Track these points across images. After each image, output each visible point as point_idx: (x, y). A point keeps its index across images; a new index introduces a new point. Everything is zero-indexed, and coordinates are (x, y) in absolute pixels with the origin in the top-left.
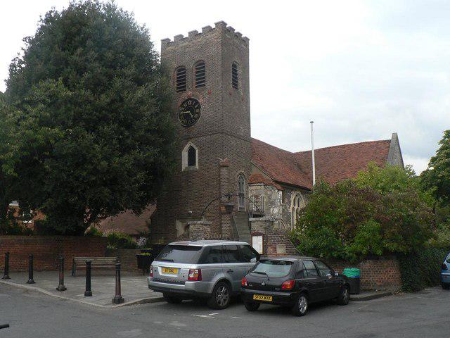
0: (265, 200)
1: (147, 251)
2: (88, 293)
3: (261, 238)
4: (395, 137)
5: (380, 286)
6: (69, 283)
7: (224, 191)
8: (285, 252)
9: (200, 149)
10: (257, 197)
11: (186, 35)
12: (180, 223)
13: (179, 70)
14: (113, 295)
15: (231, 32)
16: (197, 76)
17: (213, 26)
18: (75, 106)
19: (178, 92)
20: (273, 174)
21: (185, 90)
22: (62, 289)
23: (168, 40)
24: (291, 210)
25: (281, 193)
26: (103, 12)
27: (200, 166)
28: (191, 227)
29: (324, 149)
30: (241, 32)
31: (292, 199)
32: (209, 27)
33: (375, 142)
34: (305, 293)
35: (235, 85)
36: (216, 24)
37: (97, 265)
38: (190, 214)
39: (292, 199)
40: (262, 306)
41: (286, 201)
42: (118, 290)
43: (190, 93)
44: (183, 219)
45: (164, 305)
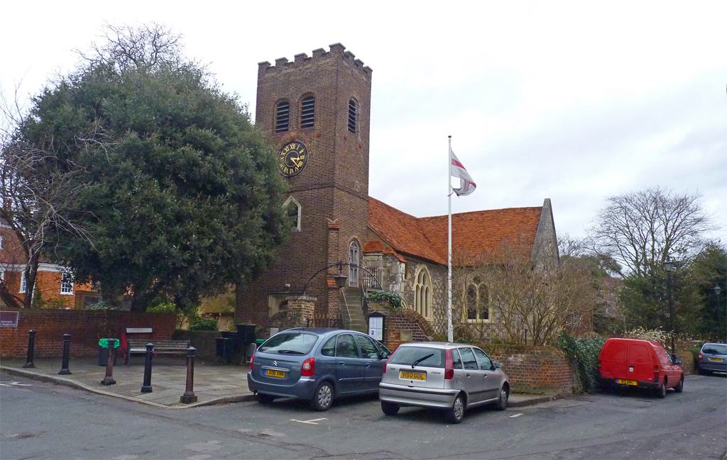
0: (383, 274)
2: (147, 388)
3: (381, 320)
4: (548, 202)
5: (535, 388)
6: (117, 374)
7: (331, 261)
10: (373, 270)
11: (291, 59)
12: (274, 300)
13: (281, 104)
14: (181, 389)
15: (350, 58)
16: (304, 113)
17: (328, 50)
18: (267, 192)
19: (277, 132)
20: (395, 242)
21: (287, 130)
22: (108, 382)
24: (414, 289)
25: (403, 265)
27: (303, 225)
28: (290, 303)
30: (353, 52)
31: (417, 275)
33: (521, 209)
34: (329, 382)
35: (352, 127)
36: (331, 47)
37: (166, 350)
38: (287, 288)
39: (417, 275)
40: (402, 410)
41: (409, 276)
42: (190, 385)
43: (293, 134)
44: (279, 293)
45: (256, 404)
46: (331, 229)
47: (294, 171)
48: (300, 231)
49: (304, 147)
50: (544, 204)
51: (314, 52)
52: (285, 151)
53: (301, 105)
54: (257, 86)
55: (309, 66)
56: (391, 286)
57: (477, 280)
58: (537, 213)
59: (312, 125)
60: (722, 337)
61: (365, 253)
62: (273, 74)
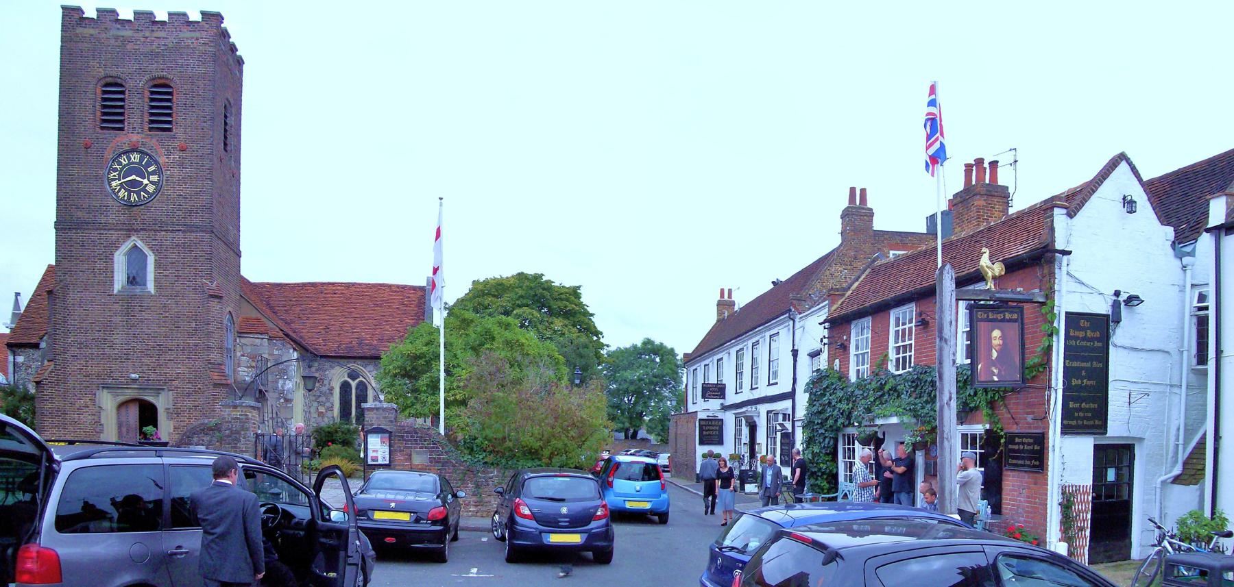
1: (1018, 444)
8: (427, 463)
9: (157, 252)
13: (107, 85)
19: (103, 128)
21: (122, 129)
23: (79, 10)
26: (984, 250)
29: (313, 285)
32: (185, 15)
43: (135, 138)
46: (211, 296)
47: (139, 196)
48: (153, 292)
49: (156, 162)
50: (1168, 224)
51: (137, 14)
52: (120, 163)
53: (147, 94)
54: (59, 44)
55: (162, 34)
56: (281, 382)
57: (353, 375)
58: (419, 293)
59: (169, 130)
60: (4, 508)
61: (241, 334)
62: (92, 31)
